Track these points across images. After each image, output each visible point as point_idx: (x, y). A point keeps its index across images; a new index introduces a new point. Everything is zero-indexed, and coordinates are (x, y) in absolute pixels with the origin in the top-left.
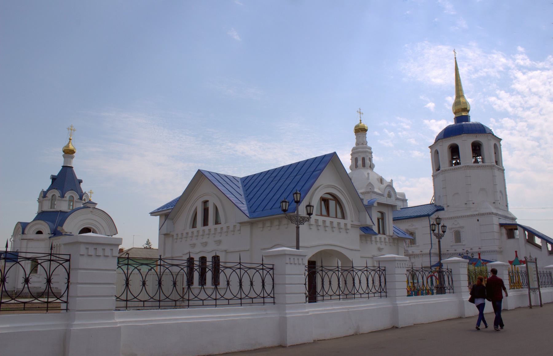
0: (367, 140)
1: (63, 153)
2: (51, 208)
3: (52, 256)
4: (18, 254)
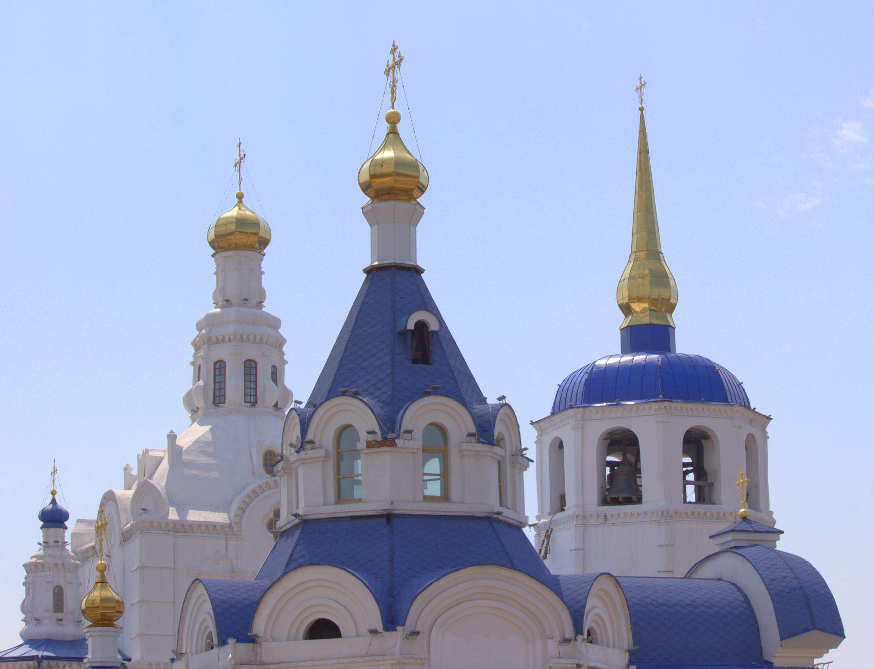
0: (265, 284)
1: (367, 199)
2: (339, 500)
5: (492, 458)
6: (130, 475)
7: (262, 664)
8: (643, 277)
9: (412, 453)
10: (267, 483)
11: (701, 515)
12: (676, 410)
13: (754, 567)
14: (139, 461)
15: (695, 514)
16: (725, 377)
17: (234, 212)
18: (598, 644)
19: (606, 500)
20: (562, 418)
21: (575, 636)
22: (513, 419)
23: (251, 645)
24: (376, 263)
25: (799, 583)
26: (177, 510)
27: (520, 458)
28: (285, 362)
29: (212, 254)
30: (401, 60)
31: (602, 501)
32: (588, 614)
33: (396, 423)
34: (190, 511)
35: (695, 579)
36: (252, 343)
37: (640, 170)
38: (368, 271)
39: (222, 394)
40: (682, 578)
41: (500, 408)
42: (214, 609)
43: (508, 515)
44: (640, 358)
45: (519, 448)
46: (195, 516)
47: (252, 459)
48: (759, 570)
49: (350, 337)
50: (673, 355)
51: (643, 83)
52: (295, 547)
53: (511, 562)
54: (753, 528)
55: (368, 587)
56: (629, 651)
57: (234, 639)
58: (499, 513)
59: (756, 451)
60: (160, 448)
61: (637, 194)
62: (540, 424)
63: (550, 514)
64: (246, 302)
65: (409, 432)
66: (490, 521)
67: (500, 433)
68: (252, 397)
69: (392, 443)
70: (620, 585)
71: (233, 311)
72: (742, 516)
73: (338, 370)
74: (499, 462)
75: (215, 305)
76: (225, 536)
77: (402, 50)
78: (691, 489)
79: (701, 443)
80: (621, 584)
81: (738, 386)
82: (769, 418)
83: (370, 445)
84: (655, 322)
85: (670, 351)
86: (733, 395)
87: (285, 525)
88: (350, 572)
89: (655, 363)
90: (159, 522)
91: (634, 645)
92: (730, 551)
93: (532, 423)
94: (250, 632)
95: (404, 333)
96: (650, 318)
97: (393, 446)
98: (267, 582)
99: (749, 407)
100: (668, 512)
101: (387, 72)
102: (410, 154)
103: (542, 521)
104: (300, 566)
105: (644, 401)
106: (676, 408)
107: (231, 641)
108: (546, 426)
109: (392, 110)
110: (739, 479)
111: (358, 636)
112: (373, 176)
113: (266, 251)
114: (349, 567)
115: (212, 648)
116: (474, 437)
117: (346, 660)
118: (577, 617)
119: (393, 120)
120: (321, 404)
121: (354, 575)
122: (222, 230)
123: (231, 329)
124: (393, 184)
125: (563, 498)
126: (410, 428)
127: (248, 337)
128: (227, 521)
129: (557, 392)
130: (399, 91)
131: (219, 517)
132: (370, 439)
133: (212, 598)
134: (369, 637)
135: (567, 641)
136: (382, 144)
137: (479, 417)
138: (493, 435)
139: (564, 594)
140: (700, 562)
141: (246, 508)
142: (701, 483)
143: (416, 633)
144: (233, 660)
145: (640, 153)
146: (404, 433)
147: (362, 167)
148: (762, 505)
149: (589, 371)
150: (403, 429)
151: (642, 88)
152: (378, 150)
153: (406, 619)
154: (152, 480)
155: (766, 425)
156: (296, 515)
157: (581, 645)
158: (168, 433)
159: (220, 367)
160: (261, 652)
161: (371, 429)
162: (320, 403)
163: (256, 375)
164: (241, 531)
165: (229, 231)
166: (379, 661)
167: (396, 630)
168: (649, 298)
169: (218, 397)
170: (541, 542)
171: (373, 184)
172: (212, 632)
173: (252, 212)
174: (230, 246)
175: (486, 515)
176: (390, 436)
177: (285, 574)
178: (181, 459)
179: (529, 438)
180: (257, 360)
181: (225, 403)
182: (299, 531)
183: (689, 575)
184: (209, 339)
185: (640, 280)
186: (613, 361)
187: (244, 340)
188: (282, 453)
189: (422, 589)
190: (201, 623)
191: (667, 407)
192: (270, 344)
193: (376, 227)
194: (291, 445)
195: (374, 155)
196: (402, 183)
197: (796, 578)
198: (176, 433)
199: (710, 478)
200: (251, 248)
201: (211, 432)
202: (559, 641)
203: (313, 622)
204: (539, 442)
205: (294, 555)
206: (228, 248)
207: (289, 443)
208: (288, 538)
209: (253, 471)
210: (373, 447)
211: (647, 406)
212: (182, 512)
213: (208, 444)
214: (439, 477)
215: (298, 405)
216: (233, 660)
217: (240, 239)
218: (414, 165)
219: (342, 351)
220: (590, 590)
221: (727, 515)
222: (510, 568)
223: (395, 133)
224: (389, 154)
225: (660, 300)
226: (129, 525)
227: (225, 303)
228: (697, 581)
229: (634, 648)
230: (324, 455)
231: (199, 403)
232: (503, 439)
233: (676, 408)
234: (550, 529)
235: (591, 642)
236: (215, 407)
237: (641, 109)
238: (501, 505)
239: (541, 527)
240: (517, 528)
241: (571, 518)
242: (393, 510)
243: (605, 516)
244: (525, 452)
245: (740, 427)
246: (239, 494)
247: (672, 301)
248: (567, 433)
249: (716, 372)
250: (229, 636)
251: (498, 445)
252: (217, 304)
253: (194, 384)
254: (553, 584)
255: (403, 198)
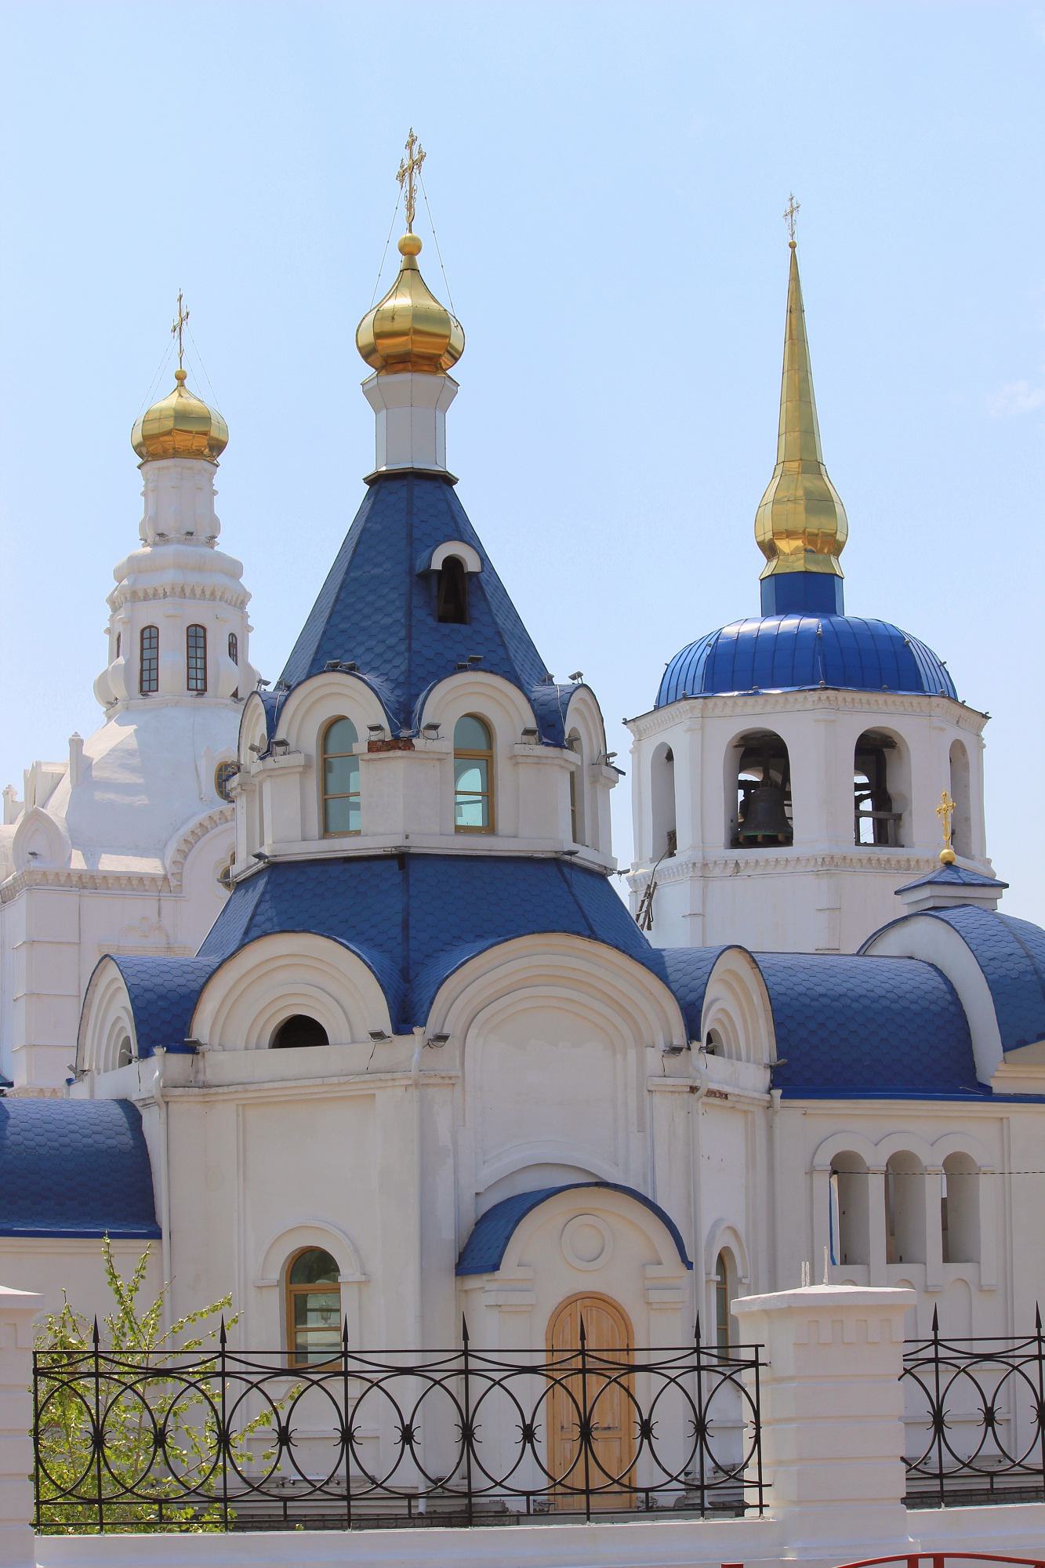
2: (326, 832)
3: (469, 1358)
4: (719, 1362)
5: (562, 767)
6: (12, 801)
7: (206, 1086)
8: (795, 501)
9: (439, 759)
10: (221, 812)
11: (883, 863)
12: (845, 702)
13: (963, 939)
14: (26, 781)
15: (873, 862)
16: (920, 654)
17: (172, 401)
18: (723, 1056)
19: (738, 839)
20: (672, 715)
21: (688, 1044)
22: (595, 712)
23: (189, 1057)
24: (384, 469)
25: (1032, 965)
26: (83, 855)
27: (604, 767)
28: (249, 629)
29: (137, 465)
30: (422, 158)
31: (732, 841)
32: (708, 1009)
33: (414, 715)
34: (103, 855)
35: (869, 956)
36: (199, 599)
37: (791, 338)
38: (372, 480)
39: (153, 677)
40: (853, 955)
41: (574, 691)
42: (132, 1001)
43: (586, 856)
44: (790, 623)
45: (603, 753)
46: (110, 863)
47: (198, 777)
48: (971, 943)
49: (344, 581)
50: (840, 618)
51: (795, 206)
52: (257, 906)
53: (593, 932)
54: (962, 879)
55: (369, 967)
56: (771, 1067)
57: (163, 1047)
58: (572, 853)
59: (966, 767)
60: (59, 759)
61: (786, 374)
62: (638, 723)
63: (652, 860)
64: (189, 537)
65: (434, 727)
66: (559, 866)
67: (574, 730)
68: (199, 681)
69: (408, 745)
70: (757, 965)
71: (169, 550)
72: (945, 861)
73: (324, 633)
74: (572, 774)
75: (143, 542)
76: (157, 894)
77: (424, 142)
78: (867, 825)
79: (883, 752)
80: (759, 963)
81: (939, 666)
82: (985, 717)
83: (373, 747)
84: (813, 569)
85: (836, 613)
86: (931, 681)
87: (244, 871)
88: (341, 944)
89: (812, 631)
90: (57, 874)
91: (779, 1058)
92: (926, 915)
93: (626, 722)
94: (189, 1037)
95: (427, 574)
96: (805, 562)
97: (409, 749)
98: (214, 960)
99: (955, 699)
100: (832, 858)
101: (401, 177)
102: (436, 301)
103: (641, 871)
104: (266, 934)
105: (797, 688)
106: (844, 699)
107: (159, 1051)
108: (646, 726)
109: (409, 235)
110: (941, 804)
111: (353, 1042)
112: (379, 336)
113: (220, 459)
114: (341, 936)
115: (130, 1062)
116: (533, 735)
117: (335, 1080)
118: (692, 1014)
119: (410, 250)
120: (299, 684)
121: (347, 948)
122: (154, 428)
123: (168, 578)
124: (410, 347)
125: (672, 837)
126: (435, 721)
127: (193, 591)
128: (160, 871)
129: (664, 675)
130: (418, 205)
131: (149, 866)
132: (373, 739)
133: (129, 985)
134: (372, 1043)
135: (675, 1050)
136: (393, 286)
137: (542, 705)
138: (564, 732)
139: (671, 978)
140: (880, 930)
141: (190, 851)
142: (882, 815)
143: (442, 1038)
144: (161, 1081)
145: (790, 312)
146: (424, 728)
147: (362, 322)
148: (975, 851)
149: (712, 642)
150: (424, 724)
151: (794, 214)
152: (386, 296)
153: (427, 1016)
154: (46, 809)
155: (981, 727)
156: (260, 856)
157: (697, 1057)
158: (70, 736)
159: (149, 637)
160: (205, 1068)
161: (374, 723)
162: (297, 682)
163: (205, 647)
164: (181, 885)
165: (166, 429)
166: (387, 1080)
167: (413, 1033)
168: (804, 532)
169: (148, 682)
170: (640, 904)
171: (379, 348)
172: (129, 1037)
173: (199, 400)
174: (165, 451)
175: (553, 855)
176: (405, 733)
177: (242, 946)
178: (91, 775)
179: (620, 742)
180: (206, 626)
181: (157, 690)
182: (265, 879)
183: (862, 952)
184: (134, 594)
185: (790, 505)
186: (749, 628)
187: (187, 595)
188: (239, 761)
189: (453, 969)
190: (110, 982)
191: (831, 699)
192: (226, 601)
193: (384, 412)
194: (252, 748)
195: (381, 304)
196: (423, 347)
197: (1028, 956)
198: (82, 738)
199: (896, 809)
200: (198, 454)
201: (136, 735)
202: (664, 1051)
203: (286, 1021)
204: (636, 751)
205: (257, 918)
206: (163, 455)
207: (249, 745)
208: (247, 891)
209: (201, 794)
210: (379, 750)
211: (800, 696)
212: (91, 856)
213: (131, 753)
214: (480, 798)
215: (263, 687)
216: (161, 1081)
217: (181, 441)
218: (443, 319)
219: (331, 604)
220: (711, 973)
221: (922, 864)
222: (589, 937)
223: (414, 270)
224: (403, 301)
225: (820, 535)
226: (11, 878)
227: (157, 538)
228: (875, 959)
229: (778, 1063)
230: (303, 764)
231: (119, 690)
232: (577, 739)
233: (844, 699)
234: (653, 883)
235: (712, 1052)
236: (142, 697)
237: (793, 246)
238: (575, 841)
239: (638, 881)
240: (599, 876)
241: (684, 867)
242: (409, 847)
243: (737, 863)
244: (611, 759)
245: (942, 729)
246: (178, 829)
247: (839, 537)
248: (680, 739)
249: (906, 646)
250: (155, 1043)
251: (571, 748)
252: (146, 541)
253: (111, 662)
254: (654, 962)
255: (426, 368)
